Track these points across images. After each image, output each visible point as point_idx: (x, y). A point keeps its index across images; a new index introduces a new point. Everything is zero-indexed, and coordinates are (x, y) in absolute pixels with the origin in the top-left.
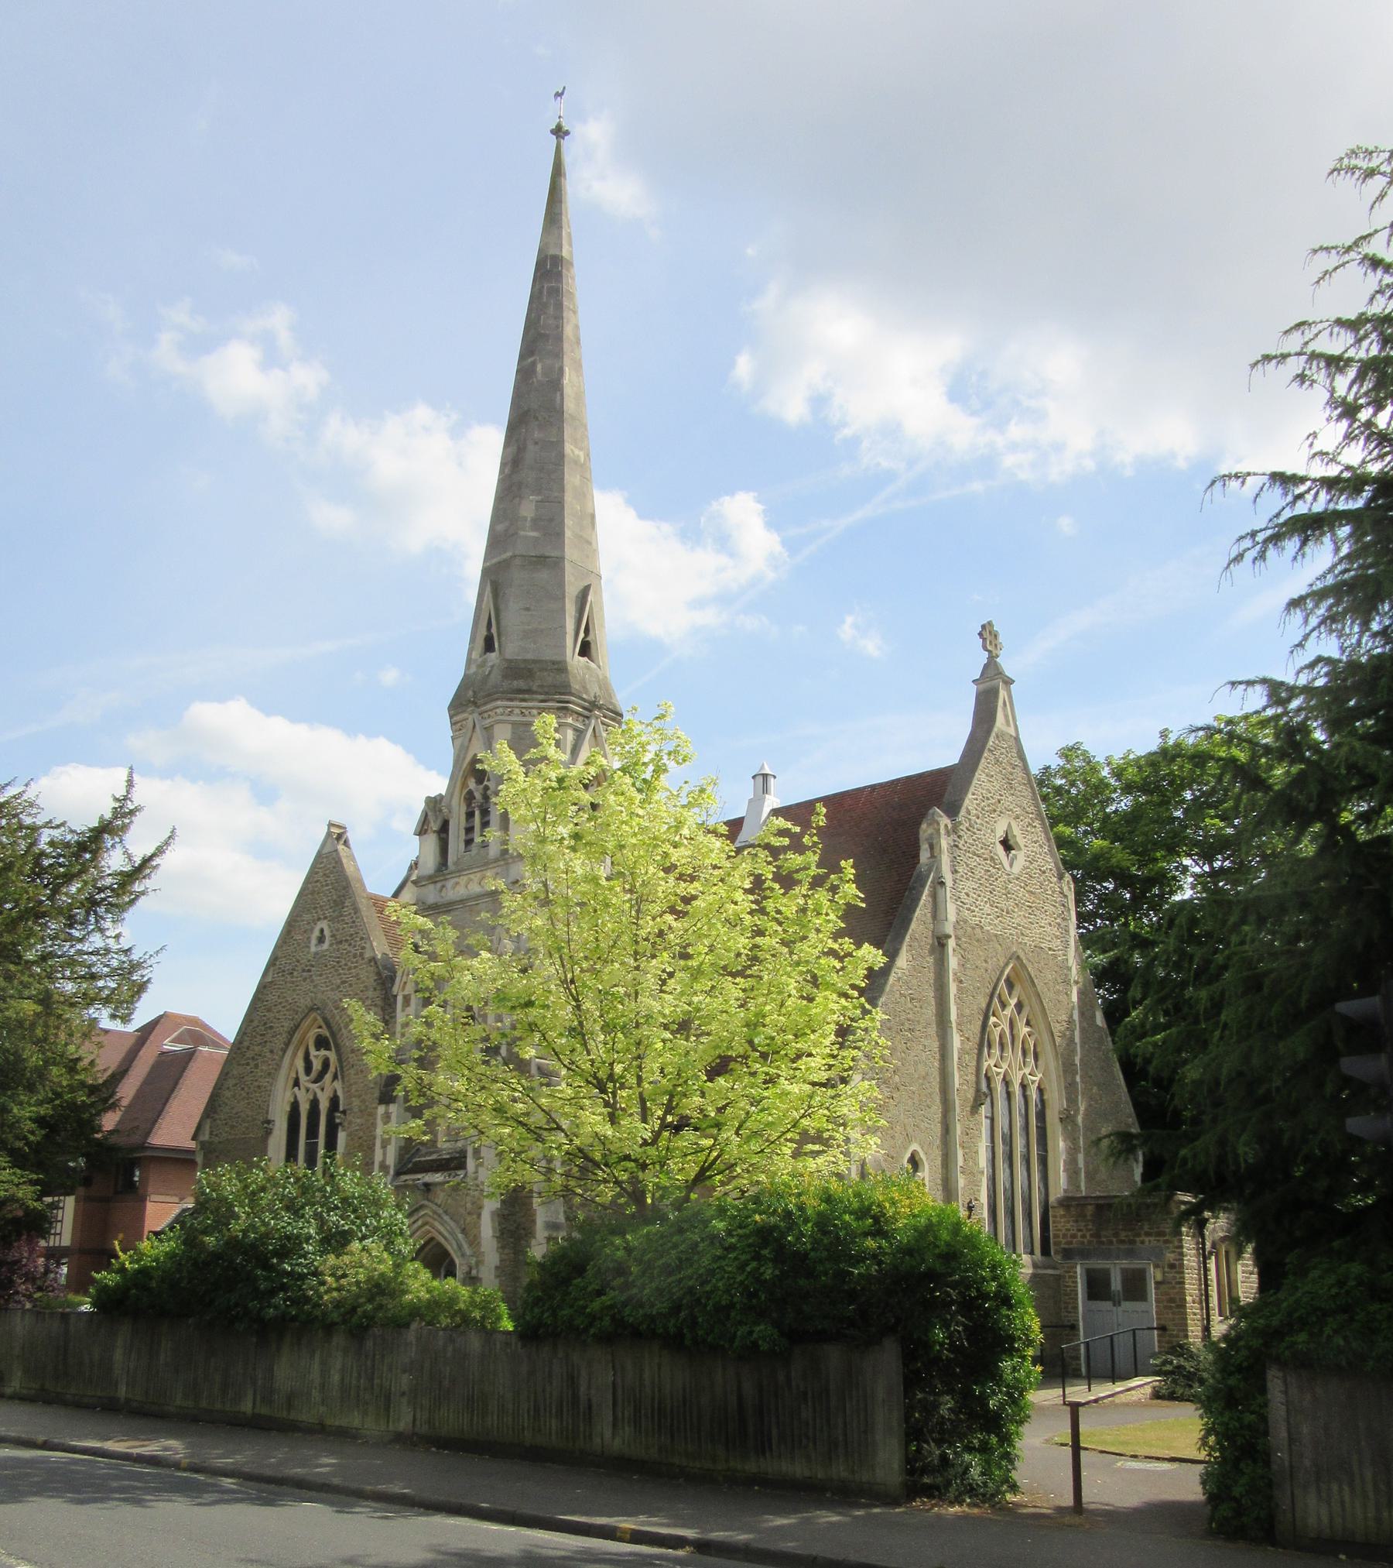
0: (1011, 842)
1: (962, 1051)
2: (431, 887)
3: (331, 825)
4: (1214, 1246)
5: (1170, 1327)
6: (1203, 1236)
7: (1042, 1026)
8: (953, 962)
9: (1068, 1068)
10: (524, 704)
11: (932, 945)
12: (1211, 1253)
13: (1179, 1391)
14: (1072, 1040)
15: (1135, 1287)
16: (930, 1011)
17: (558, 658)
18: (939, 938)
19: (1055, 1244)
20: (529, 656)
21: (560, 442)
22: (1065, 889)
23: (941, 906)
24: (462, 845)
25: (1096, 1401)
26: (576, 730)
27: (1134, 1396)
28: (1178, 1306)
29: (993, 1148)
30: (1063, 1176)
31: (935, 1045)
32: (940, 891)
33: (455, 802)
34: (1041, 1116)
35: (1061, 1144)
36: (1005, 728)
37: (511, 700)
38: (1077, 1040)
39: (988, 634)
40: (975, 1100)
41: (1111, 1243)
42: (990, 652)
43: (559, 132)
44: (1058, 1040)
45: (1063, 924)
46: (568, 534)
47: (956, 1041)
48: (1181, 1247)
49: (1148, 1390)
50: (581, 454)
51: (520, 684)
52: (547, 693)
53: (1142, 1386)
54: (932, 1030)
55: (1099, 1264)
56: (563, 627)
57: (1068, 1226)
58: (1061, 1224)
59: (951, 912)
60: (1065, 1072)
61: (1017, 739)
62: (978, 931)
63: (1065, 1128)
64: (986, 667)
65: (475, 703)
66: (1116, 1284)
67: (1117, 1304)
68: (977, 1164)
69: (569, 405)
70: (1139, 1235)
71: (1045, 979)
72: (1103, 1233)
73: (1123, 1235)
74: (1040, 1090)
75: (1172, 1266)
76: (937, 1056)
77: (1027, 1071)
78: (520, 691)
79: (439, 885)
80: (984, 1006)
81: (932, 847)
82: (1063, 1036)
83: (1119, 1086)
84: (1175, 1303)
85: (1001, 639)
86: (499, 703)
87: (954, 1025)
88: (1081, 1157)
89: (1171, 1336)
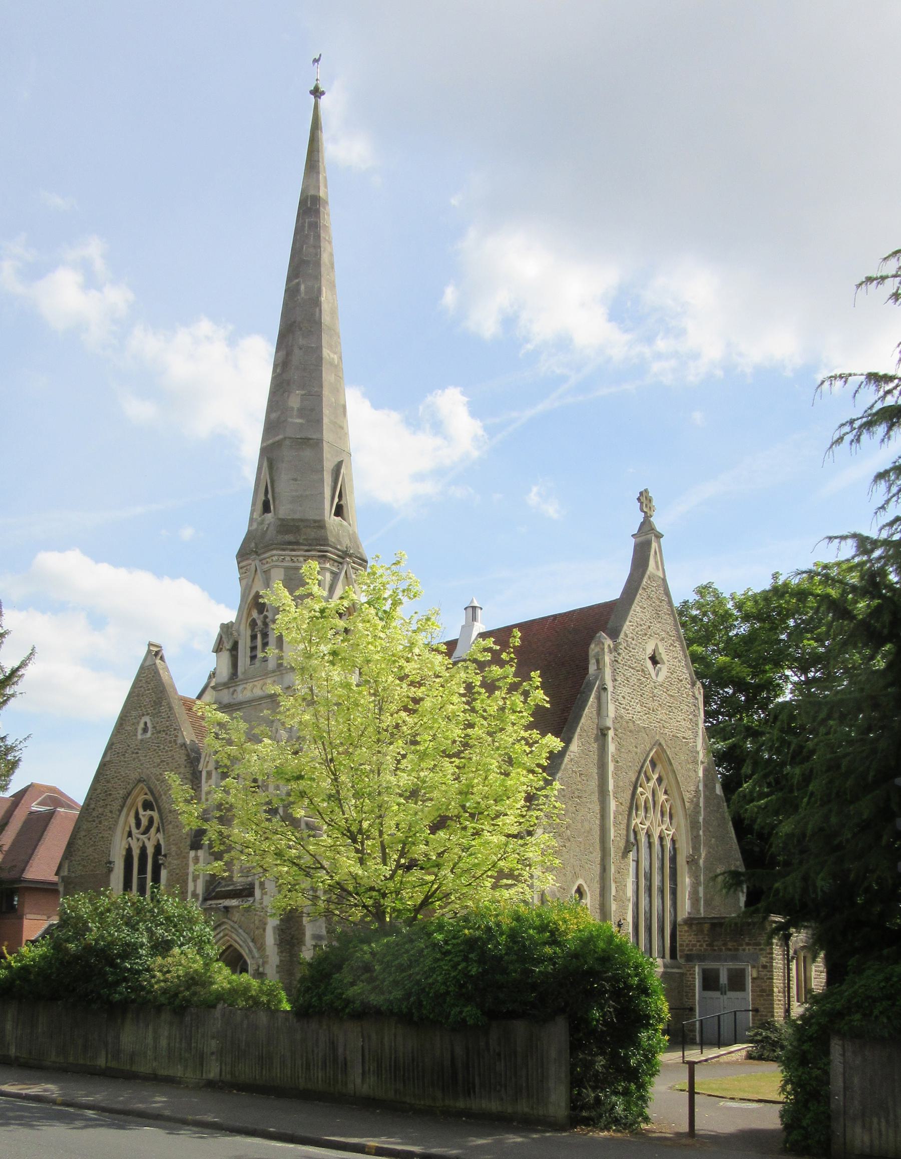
0: (658, 658)
1: (617, 813)
2: (226, 691)
3: (150, 645)
4: (795, 952)
8: (612, 748)
9: (694, 825)
10: (294, 553)
11: (597, 735)
12: (793, 958)
13: (766, 1054)
14: (697, 805)
15: (737, 982)
16: (594, 784)
17: (318, 518)
18: (601, 730)
20: (297, 516)
21: (319, 348)
22: (697, 693)
23: (604, 706)
24: (248, 660)
25: (706, 1060)
26: (332, 573)
27: (734, 1057)
28: (768, 995)
31: (597, 808)
32: (603, 694)
33: (242, 627)
35: (687, 880)
37: (284, 550)
38: (701, 805)
40: (626, 848)
43: (317, 92)
45: (694, 719)
46: (326, 420)
47: (613, 805)
48: (772, 953)
49: (744, 1053)
50: (336, 357)
51: (289, 537)
52: (310, 545)
53: (739, 1050)
54: (595, 797)
55: (711, 965)
56: (322, 493)
57: (690, 938)
60: (692, 828)
62: (631, 724)
63: (690, 869)
65: (256, 552)
66: (724, 979)
67: (724, 993)
69: (326, 319)
70: (742, 945)
71: (679, 760)
73: (730, 945)
74: (673, 841)
75: (764, 967)
76: (598, 816)
77: (664, 827)
78: (290, 543)
79: (231, 690)
80: (634, 779)
81: (598, 662)
86: (274, 552)
87: (611, 794)
88: (701, 889)
89: (761, 1016)
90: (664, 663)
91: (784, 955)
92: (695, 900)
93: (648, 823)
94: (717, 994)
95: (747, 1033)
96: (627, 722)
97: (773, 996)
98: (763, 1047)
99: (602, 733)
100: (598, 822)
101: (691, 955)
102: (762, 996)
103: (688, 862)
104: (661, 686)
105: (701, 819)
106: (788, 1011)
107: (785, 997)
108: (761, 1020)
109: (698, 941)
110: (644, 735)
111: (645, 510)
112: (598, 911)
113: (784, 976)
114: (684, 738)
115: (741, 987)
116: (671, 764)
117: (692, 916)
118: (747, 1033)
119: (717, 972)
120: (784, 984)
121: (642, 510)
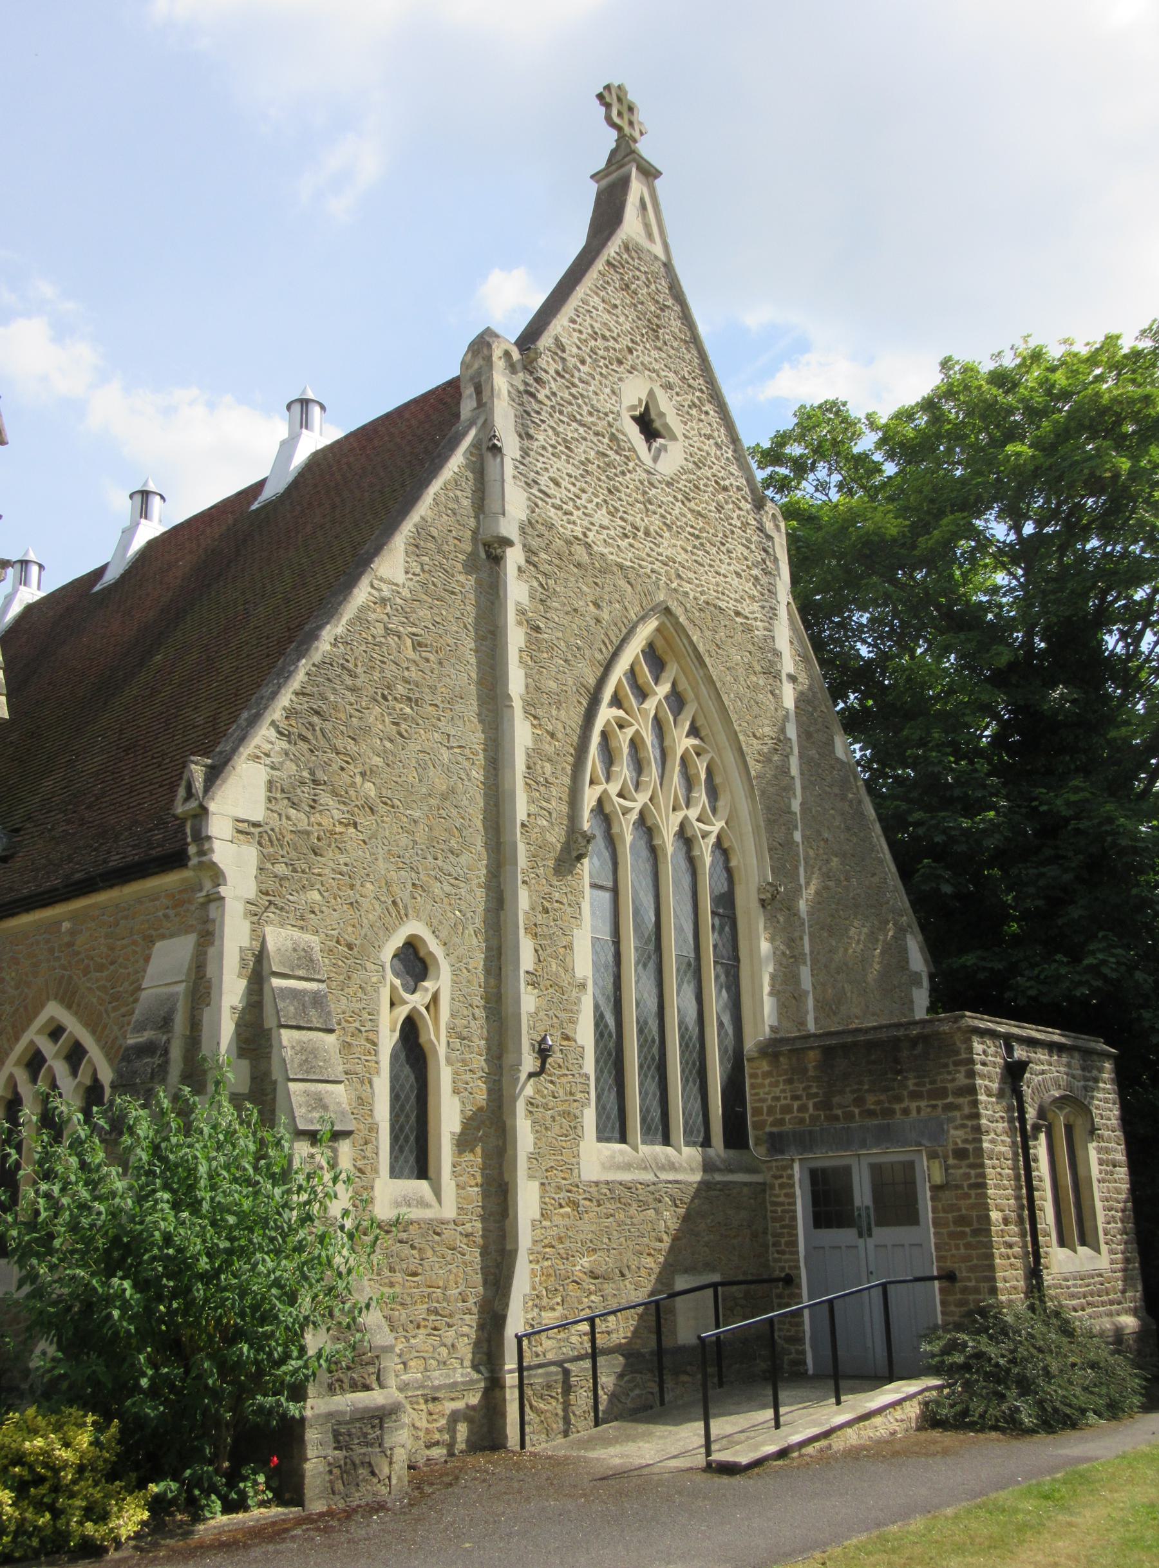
0: (657, 424)
1: (535, 755)
4: (1042, 1113)
5: (962, 1272)
6: (1018, 1095)
7: (722, 738)
8: (517, 591)
9: (776, 817)
11: (472, 556)
12: (1037, 1128)
13: (977, 1407)
14: (784, 770)
15: (896, 1203)
16: (464, 674)
18: (487, 546)
19: (755, 1127)
22: (769, 526)
23: (492, 489)
25: (783, 1453)
27: (881, 1427)
28: (976, 1232)
29: (617, 943)
30: (768, 1005)
31: (476, 738)
32: (492, 463)
34: (726, 903)
35: (765, 947)
36: (641, 239)
38: (795, 771)
39: (614, 103)
40: (567, 847)
41: (849, 1117)
42: (619, 128)
44: (755, 768)
45: (764, 580)
47: (522, 734)
48: (977, 1116)
49: (913, 1410)
53: (895, 1405)
54: (470, 708)
55: (828, 1158)
57: (777, 1091)
58: (764, 1091)
59: (515, 505)
60: (771, 823)
61: (668, 266)
62: (580, 552)
63: (771, 919)
64: (613, 153)
66: (862, 1195)
67: (865, 1232)
68: (569, 970)
70: (898, 1099)
71: (728, 665)
72: (836, 1100)
73: (871, 1100)
74: (721, 848)
75: (961, 1154)
76: (480, 759)
77: (693, 813)
80: (592, 681)
81: (479, 391)
82: (766, 759)
83: (881, 861)
84: (972, 1227)
85: (641, 116)
87: (517, 705)
88: (805, 973)
89: (965, 1290)
90: (674, 438)
91: (1011, 1121)
92: (788, 992)
93: (642, 798)
94: (845, 1236)
95: (925, 1347)
96: (568, 543)
97: (988, 1232)
98: (967, 1385)
99: (489, 554)
100: (477, 774)
101: (780, 1135)
102: (963, 1235)
103: (763, 903)
104: (669, 484)
105: (796, 805)
106: (1034, 1273)
107: (1023, 1235)
108: (960, 1304)
109: (795, 1098)
110: (622, 583)
111: (617, 120)
112: (480, 1013)
113: (1017, 1178)
114: (738, 614)
115: (909, 1215)
116: (702, 663)
117: (782, 1034)
118: (925, 1347)
119: (845, 1172)
120: (1018, 1198)
121: (613, 125)
